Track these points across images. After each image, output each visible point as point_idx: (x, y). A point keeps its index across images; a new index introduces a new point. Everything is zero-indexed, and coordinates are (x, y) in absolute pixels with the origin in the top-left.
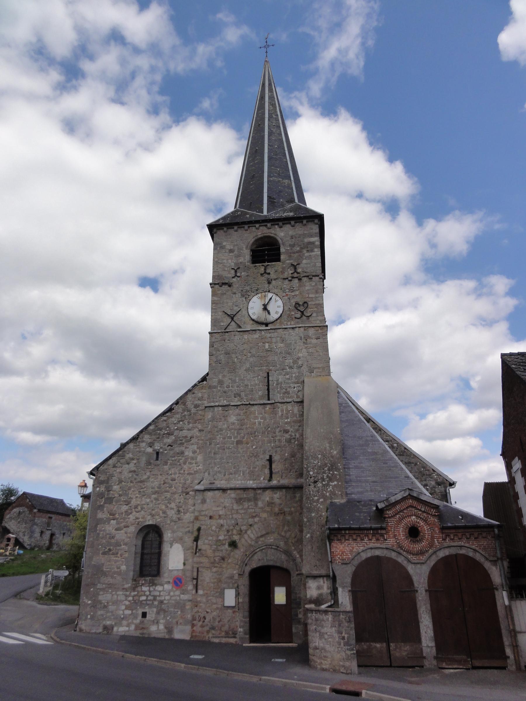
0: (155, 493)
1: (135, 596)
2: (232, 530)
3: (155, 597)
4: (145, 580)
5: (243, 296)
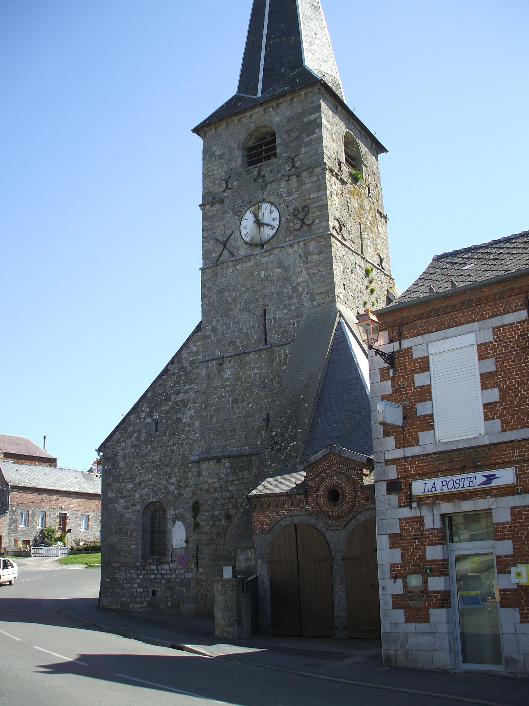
0: (156, 467)
1: (145, 574)
2: (228, 503)
3: (162, 575)
4: (153, 559)
5: (235, 214)
